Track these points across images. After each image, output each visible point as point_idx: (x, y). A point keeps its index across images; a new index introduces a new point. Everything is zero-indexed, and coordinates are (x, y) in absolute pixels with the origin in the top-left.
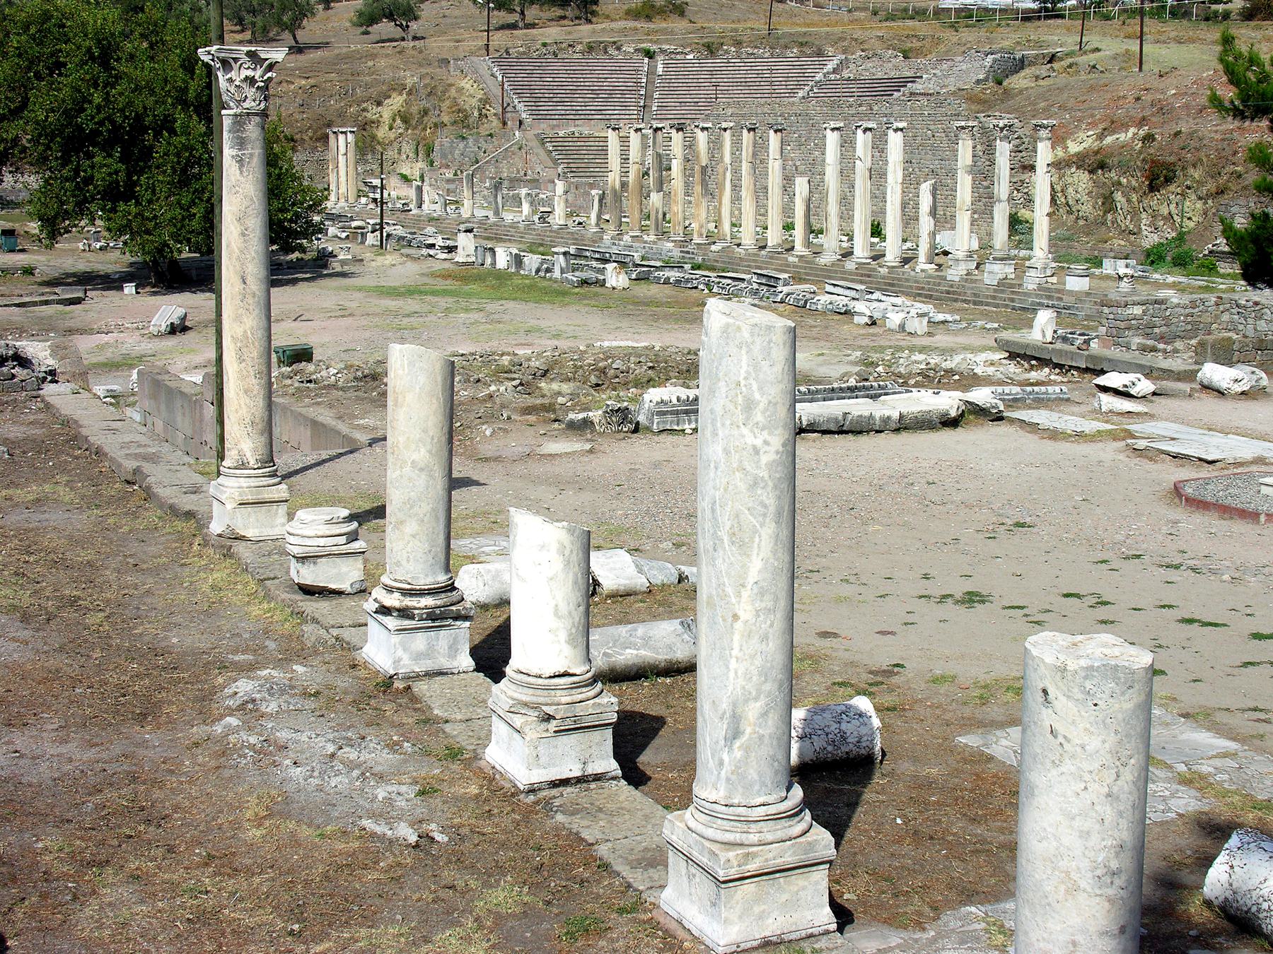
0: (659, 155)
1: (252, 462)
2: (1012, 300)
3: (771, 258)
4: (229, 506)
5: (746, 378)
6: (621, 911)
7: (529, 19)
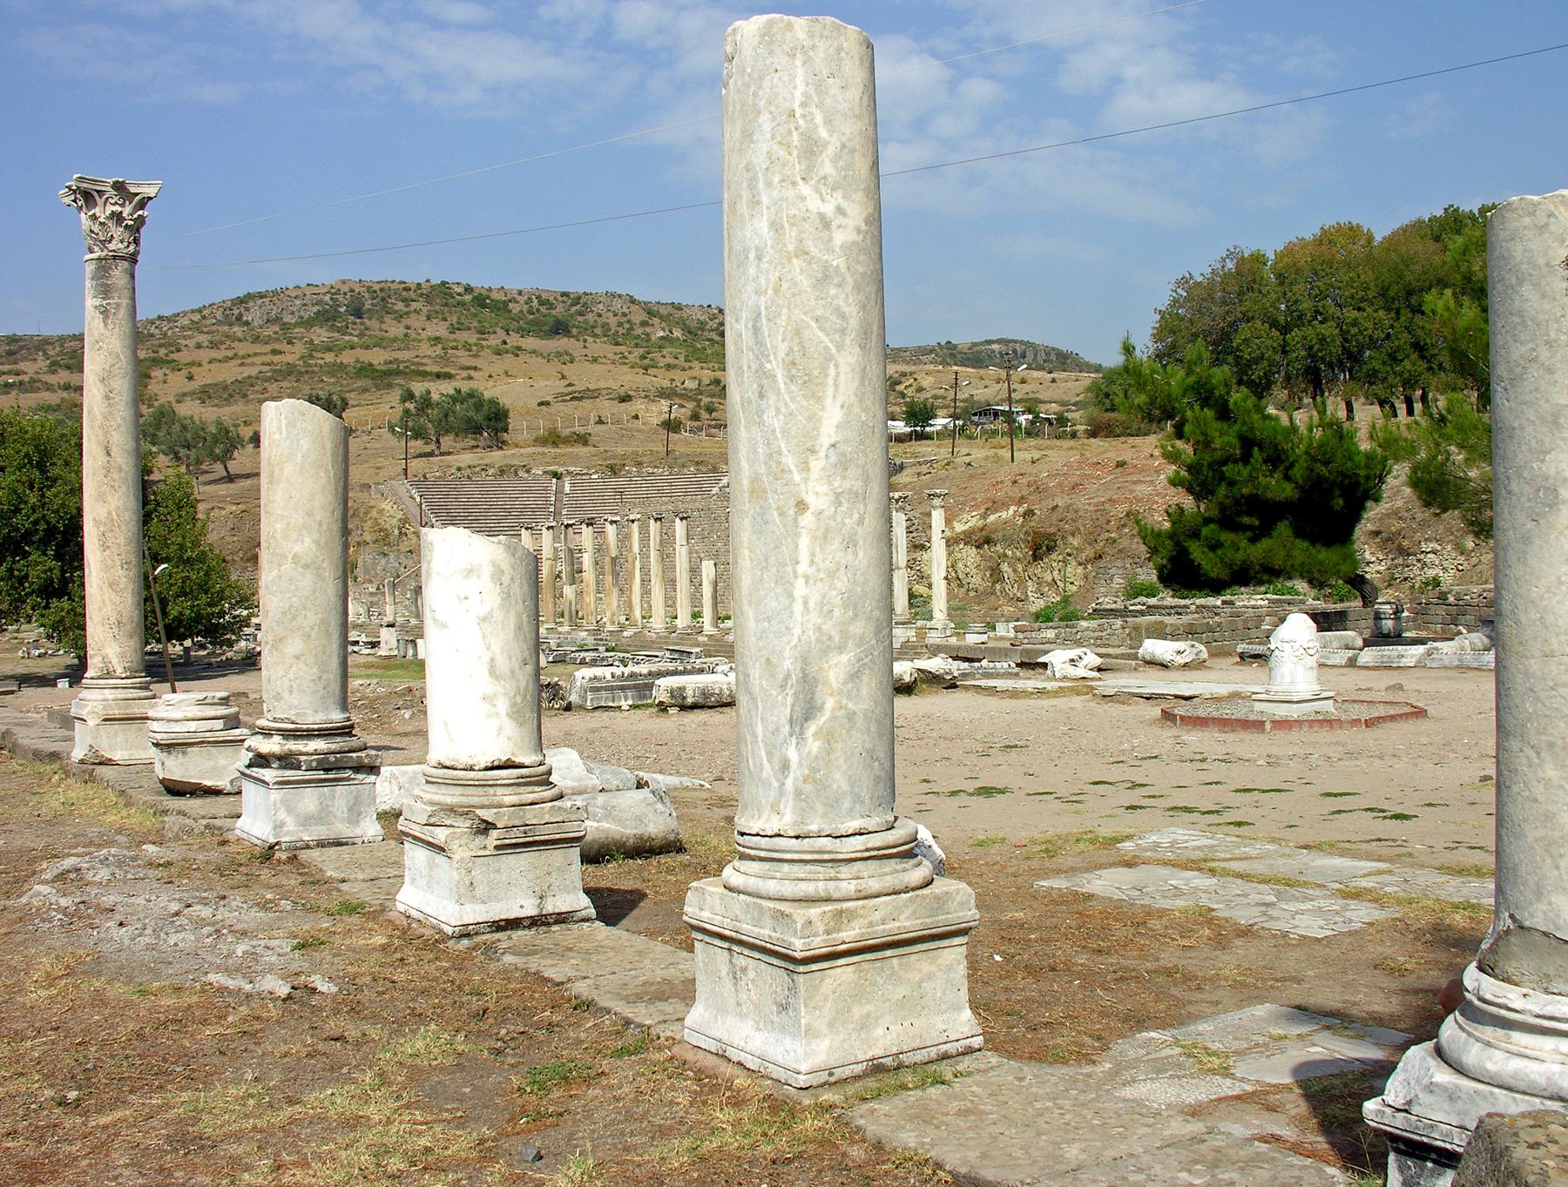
0: (570, 550)
1: (119, 670)
4: (91, 723)
5: (804, 105)
6: (620, 1053)
7: (444, 448)
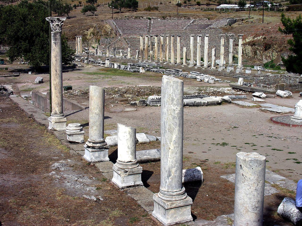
0: (152, 42)
2: (233, 76)
3: (178, 66)
4: (53, 123)
5: (172, 94)
6: (143, 216)
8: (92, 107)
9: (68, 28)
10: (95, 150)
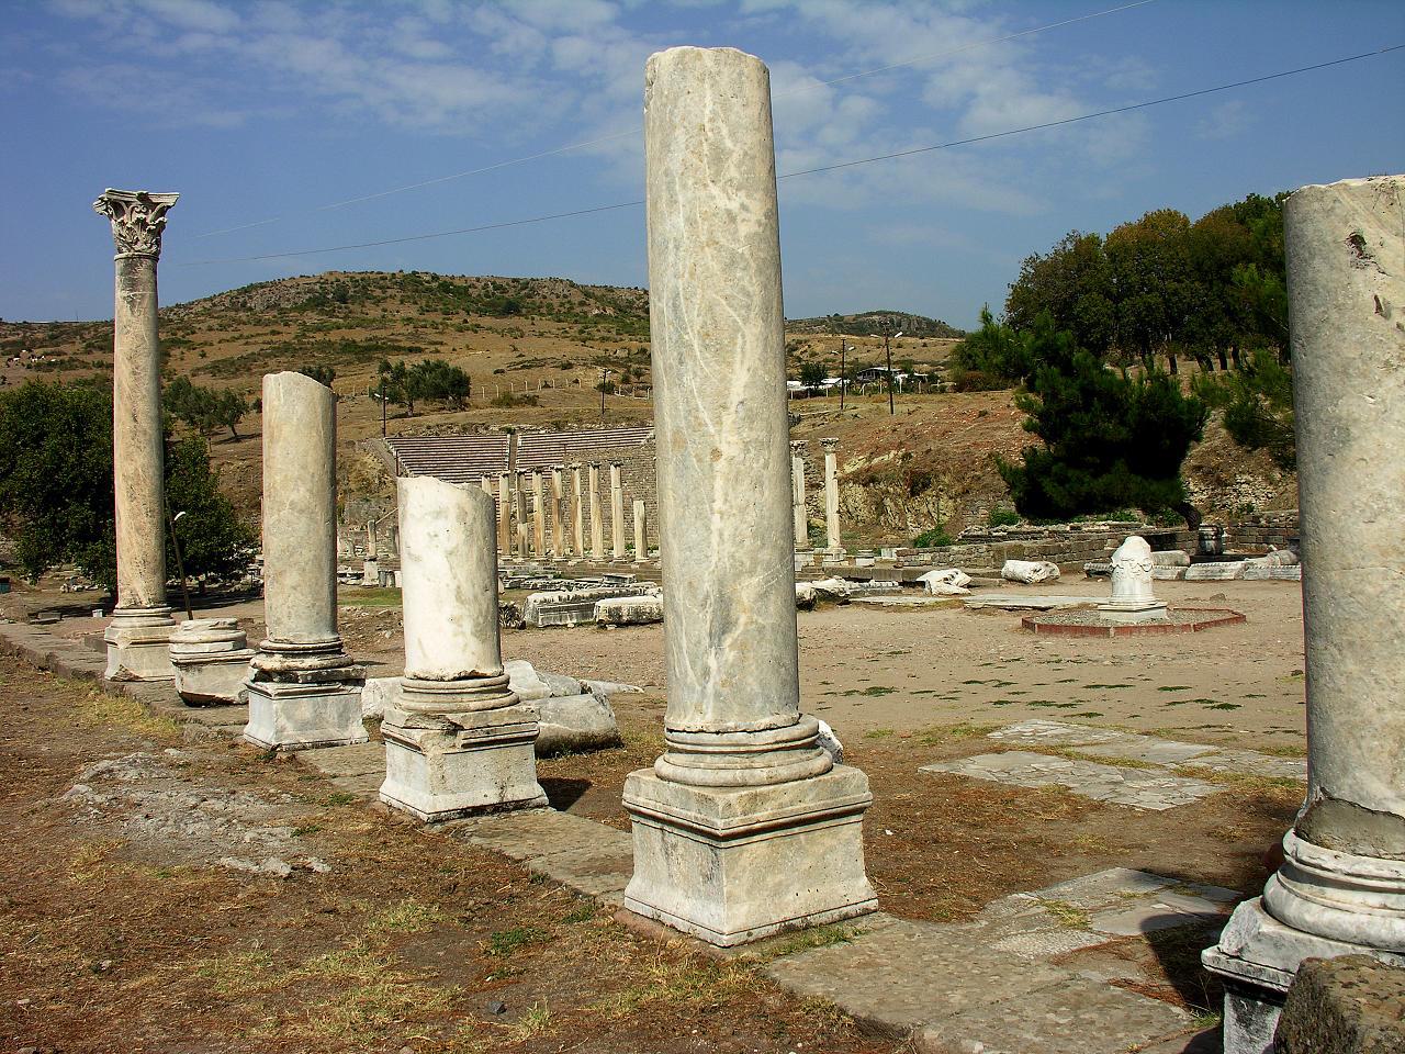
0: (523, 494)
5: (711, 120)
6: (570, 920)
8: (277, 478)
9: (234, 472)
10: (297, 685)
